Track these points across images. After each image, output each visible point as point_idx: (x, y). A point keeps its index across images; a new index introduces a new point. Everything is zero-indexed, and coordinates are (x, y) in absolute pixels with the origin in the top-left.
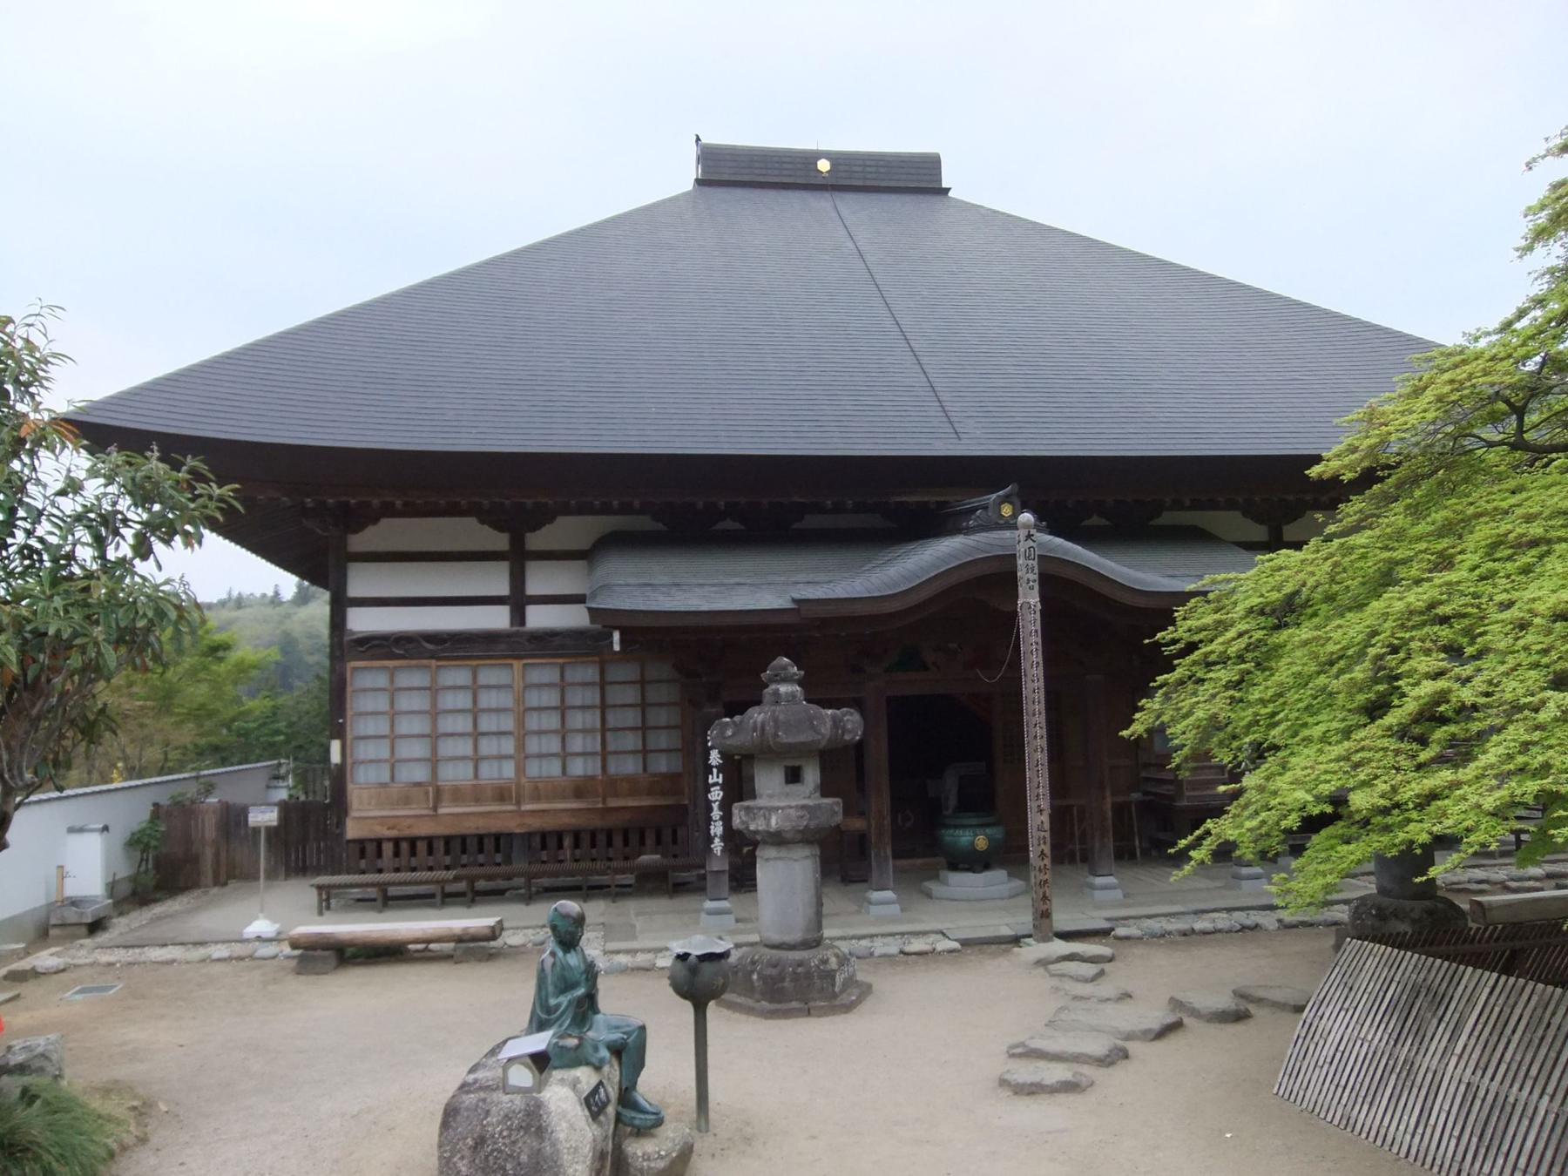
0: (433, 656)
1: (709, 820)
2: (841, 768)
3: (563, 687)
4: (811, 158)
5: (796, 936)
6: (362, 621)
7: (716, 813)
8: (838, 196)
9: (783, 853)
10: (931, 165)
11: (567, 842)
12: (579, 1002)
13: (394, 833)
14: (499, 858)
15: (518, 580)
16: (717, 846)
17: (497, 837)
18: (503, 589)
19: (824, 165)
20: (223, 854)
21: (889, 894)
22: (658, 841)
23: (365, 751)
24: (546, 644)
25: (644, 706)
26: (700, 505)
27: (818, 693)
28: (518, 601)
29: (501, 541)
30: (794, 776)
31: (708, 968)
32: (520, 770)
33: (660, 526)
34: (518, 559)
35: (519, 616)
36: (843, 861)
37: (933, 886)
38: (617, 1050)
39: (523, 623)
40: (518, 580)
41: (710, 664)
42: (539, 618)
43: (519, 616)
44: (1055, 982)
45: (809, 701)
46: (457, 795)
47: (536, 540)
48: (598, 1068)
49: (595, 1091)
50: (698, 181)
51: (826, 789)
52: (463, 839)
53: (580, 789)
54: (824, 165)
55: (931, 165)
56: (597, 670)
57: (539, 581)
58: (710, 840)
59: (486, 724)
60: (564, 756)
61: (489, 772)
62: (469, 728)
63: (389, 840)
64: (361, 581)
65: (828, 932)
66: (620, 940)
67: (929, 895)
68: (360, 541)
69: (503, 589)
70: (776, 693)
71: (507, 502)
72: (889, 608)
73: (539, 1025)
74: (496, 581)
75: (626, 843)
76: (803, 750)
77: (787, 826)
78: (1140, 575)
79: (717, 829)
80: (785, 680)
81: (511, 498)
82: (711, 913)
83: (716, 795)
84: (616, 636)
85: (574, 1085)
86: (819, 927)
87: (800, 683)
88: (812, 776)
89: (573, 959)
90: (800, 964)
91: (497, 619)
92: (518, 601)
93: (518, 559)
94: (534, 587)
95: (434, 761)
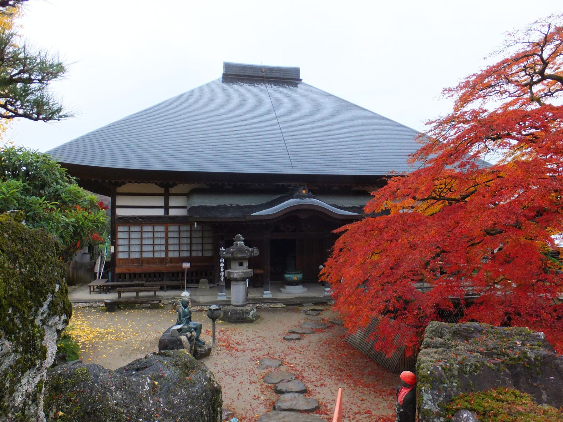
1: (220, 271)
2: (253, 263)
3: (179, 231)
5: (240, 303)
6: (120, 212)
7: (222, 270)
10: (296, 71)
11: (180, 275)
12: (188, 319)
13: (129, 272)
14: (160, 279)
15: (167, 202)
16: (222, 278)
17: (160, 274)
20: (75, 274)
21: (269, 292)
22: (206, 275)
23: (120, 249)
24: (176, 220)
25: (202, 237)
26: (220, 184)
28: (167, 207)
29: (162, 190)
30: (241, 264)
31: (215, 312)
32: (167, 254)
34: (167, 195)
35: (167, 212)
36: (256, 282)
37: (282, 290)
38: (195, 329)
39: (168, 213)
40: (167, 202)
41: (220, 231)
42: (173, 212)
43: (167, 212)
44: (307, 316)
46: (148, 261)
47: (172, 190)
48: (191, 333)
49: (191, 337)
51: (249, 267)
52: (150, 274)
55: (296, 71)
56: (189, 227)
58: (220, 277)
59: (157, 242)
61: (157, 255)
62: (152, 243)
63: (128, 274)
64: (120, 201)
67: (281, 292)
68: (120, 190)
70: (237, 244)
72: (272, 217)
73: (178, 324)
75: (197, 275)
76: (244, 259)
77: (239, 277)
79: (222, 274)
80: (240, 240)
81: (165, 182)
83: (222, 265)
84: (196, 224)
85: (187, 335)
87: (243, 241)
88: (246, 264)
89: (186, 310)
91: (160, 212)
92: (167, 207)
93: (167, 195)
94: (171, 204)
95: (141, 252)
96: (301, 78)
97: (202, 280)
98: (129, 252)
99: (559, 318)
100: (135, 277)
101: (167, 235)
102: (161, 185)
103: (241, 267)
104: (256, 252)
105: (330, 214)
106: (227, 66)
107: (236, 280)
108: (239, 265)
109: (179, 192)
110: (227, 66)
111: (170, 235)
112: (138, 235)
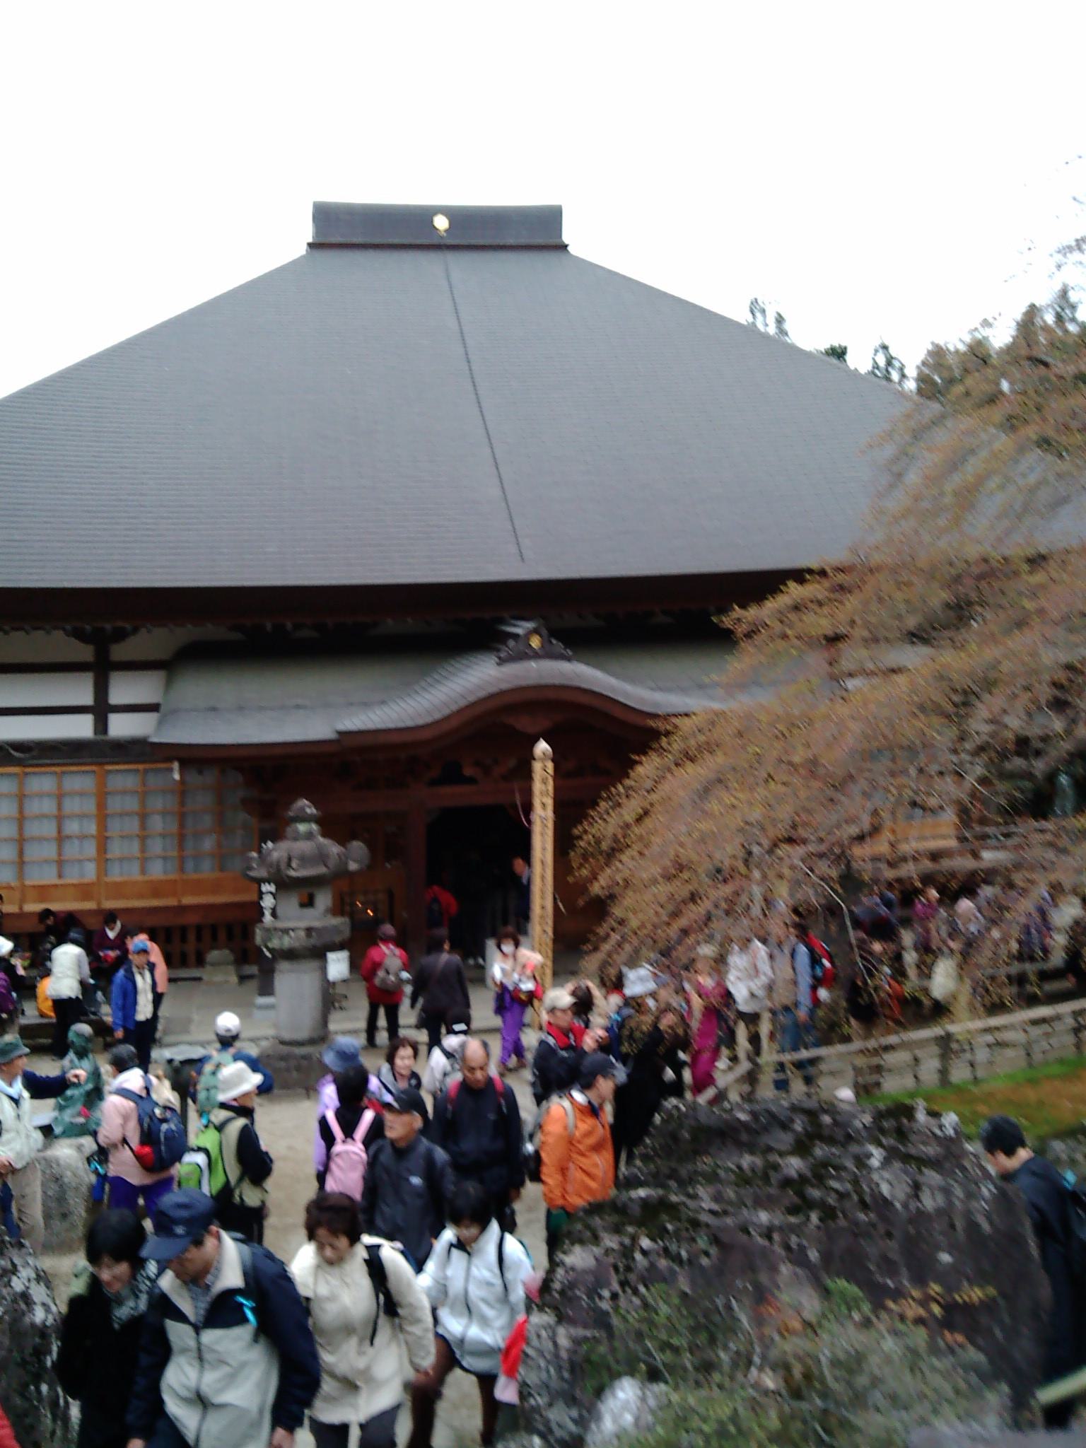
0: (19, 763)
4: (423, 216)
5: (303, 1034)
8: (451, 257)
9: (295, 965)
10: (550, 218)
11: (192, 937)
15: (101, 690)
18: (87, 699)
19: (441, 223)
26: (269, 626)
27: (331, 827)
28: (101, 710)
29: (85, 653)
30: (308, 903)
33: (236, 636)
34: (102, 670)
35: (101, 725)
40: (101, 690)
41: (265, 782)
42: (121, 727)
43: (101, 725)
45: (324, 835)
47: (119, 652)
50: (310, 245)
53: (156, 889)
54: (441, 223)
55: (550, 218)
57: (123, 690)
60: (144, 861)
61: (72, 876)
65: (332, 1027)
66: (528, 808)
69: (87, 699)
70: (297, 831)
71: (88, 627)
74: (80, 691)
75: (199, 938)
78: (628, 688)
82: (261, 1007)
86: (325, 1022)
88: (324, 900)
90: (304, 1057)
91: (81, 728)
92: (101, 710)
93: (102, 670)
96: (566, 242)
97: (214, 955)
98: (60, 863)
99: (707, 1439)
100: (214, 937)
101: (101, 806)
102: (79, 635)
103: (309, 912)
104: (356, 855)
105: (618, 713)
106: (325, 215)
107: (291, 955)
108: (303, 905)
109: (152, 658)
110: (325, 215)
111: (115, 804)
112: (48, 806)
